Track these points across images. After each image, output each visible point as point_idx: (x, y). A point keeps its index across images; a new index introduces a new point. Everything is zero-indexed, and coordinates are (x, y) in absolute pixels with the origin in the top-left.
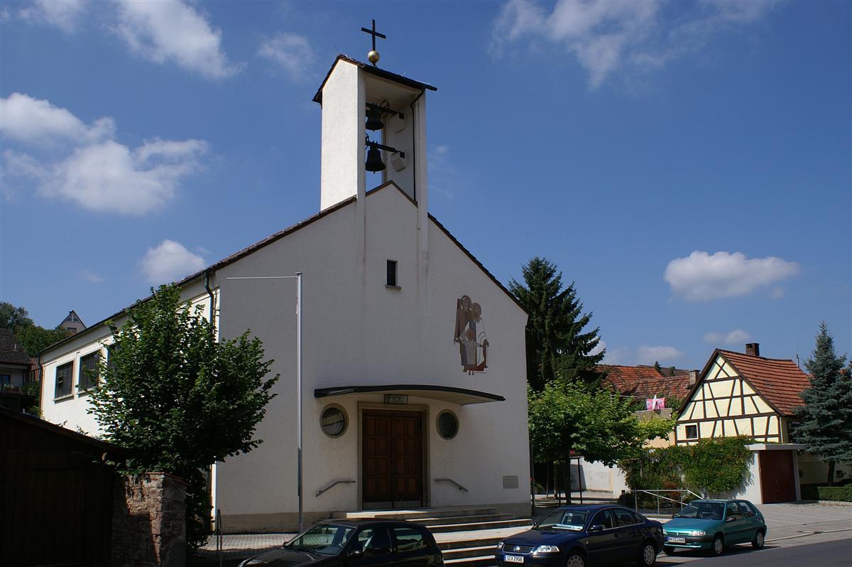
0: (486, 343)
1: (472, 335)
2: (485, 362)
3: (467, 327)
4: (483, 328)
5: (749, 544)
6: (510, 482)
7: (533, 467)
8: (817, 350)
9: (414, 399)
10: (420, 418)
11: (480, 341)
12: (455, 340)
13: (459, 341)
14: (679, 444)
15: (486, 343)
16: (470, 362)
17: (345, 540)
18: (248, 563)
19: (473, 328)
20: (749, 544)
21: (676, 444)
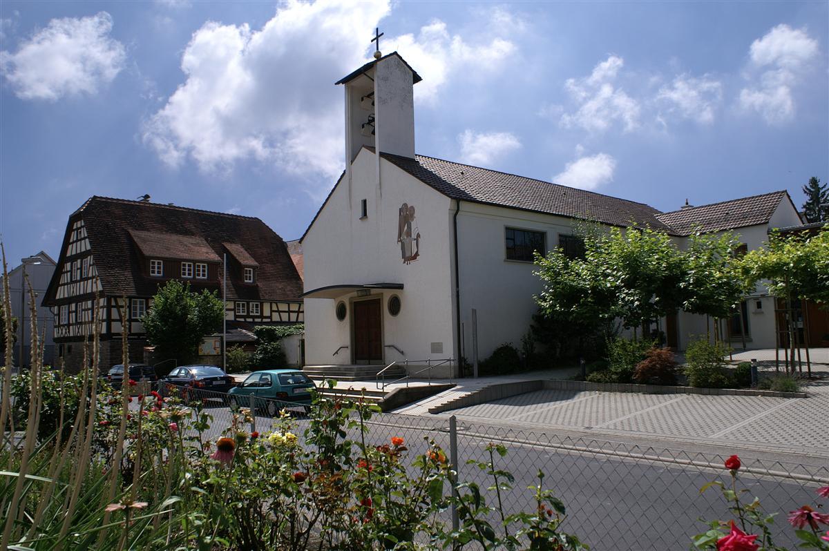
0: (418, 236)
1: (409, 234)
2: (417, 252)
3: (406, 228)
4: (416, 225)
5: (220, 400)
6: (437, 348)
7: (779, 338)
8: (294, 150)
9: (373, 291)
10: (377, 303)
11: (414, 236)
12: (398, 241)
13: (401, 241)
14: (238, 319)
15: (418, 236)
16: (408, 254)
17: (99, 360)
18: (178, 370)
19: (409, 228)
20: (220, 400)
21: (235, 319)
